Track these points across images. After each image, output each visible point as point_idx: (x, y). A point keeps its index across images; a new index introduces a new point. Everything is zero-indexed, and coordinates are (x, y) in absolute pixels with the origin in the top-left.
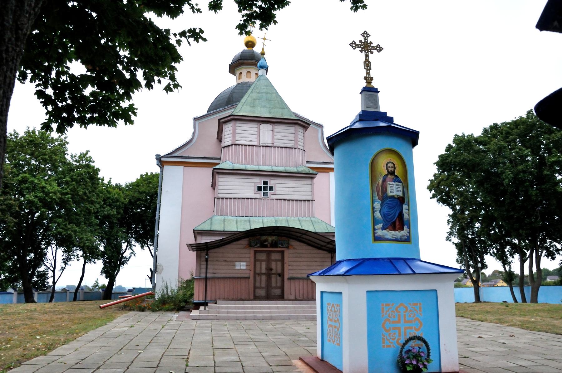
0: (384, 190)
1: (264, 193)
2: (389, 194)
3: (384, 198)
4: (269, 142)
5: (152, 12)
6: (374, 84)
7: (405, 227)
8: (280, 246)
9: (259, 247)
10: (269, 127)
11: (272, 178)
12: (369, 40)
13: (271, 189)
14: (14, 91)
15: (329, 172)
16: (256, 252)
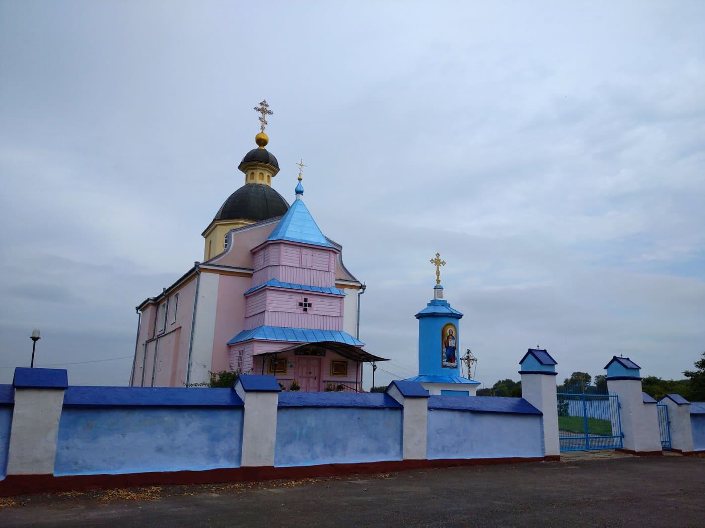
0: (447, 342)
1: (304, 308)
3: (447, 347)
4: (309, 265)
5: (516, 382)
6: (441, 284)
8: (319, 354)
9: (302, 354)
10: (309, 252)
12: (440, 258)
13: (310, 305)
15: (344, 288)
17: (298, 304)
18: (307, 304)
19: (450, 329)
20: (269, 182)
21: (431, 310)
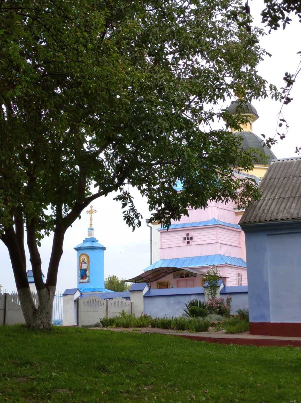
2: (82, 268)
7: (87, 278)
9: (179, 278)
11: (192, 231)
14: (250, 10)
16: (177, 281)
17: (183, 239)
18: (189, 239)
19: (83, 257)
20: (251, 128)
21: (88, 245)
